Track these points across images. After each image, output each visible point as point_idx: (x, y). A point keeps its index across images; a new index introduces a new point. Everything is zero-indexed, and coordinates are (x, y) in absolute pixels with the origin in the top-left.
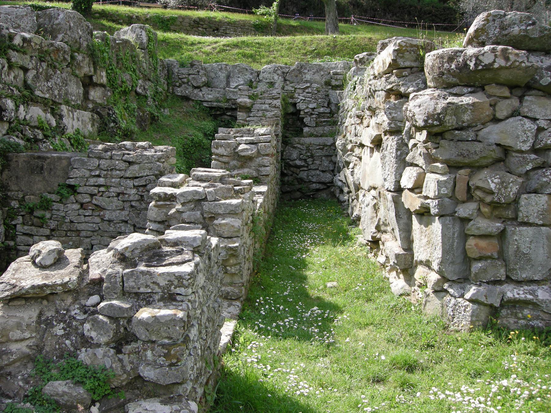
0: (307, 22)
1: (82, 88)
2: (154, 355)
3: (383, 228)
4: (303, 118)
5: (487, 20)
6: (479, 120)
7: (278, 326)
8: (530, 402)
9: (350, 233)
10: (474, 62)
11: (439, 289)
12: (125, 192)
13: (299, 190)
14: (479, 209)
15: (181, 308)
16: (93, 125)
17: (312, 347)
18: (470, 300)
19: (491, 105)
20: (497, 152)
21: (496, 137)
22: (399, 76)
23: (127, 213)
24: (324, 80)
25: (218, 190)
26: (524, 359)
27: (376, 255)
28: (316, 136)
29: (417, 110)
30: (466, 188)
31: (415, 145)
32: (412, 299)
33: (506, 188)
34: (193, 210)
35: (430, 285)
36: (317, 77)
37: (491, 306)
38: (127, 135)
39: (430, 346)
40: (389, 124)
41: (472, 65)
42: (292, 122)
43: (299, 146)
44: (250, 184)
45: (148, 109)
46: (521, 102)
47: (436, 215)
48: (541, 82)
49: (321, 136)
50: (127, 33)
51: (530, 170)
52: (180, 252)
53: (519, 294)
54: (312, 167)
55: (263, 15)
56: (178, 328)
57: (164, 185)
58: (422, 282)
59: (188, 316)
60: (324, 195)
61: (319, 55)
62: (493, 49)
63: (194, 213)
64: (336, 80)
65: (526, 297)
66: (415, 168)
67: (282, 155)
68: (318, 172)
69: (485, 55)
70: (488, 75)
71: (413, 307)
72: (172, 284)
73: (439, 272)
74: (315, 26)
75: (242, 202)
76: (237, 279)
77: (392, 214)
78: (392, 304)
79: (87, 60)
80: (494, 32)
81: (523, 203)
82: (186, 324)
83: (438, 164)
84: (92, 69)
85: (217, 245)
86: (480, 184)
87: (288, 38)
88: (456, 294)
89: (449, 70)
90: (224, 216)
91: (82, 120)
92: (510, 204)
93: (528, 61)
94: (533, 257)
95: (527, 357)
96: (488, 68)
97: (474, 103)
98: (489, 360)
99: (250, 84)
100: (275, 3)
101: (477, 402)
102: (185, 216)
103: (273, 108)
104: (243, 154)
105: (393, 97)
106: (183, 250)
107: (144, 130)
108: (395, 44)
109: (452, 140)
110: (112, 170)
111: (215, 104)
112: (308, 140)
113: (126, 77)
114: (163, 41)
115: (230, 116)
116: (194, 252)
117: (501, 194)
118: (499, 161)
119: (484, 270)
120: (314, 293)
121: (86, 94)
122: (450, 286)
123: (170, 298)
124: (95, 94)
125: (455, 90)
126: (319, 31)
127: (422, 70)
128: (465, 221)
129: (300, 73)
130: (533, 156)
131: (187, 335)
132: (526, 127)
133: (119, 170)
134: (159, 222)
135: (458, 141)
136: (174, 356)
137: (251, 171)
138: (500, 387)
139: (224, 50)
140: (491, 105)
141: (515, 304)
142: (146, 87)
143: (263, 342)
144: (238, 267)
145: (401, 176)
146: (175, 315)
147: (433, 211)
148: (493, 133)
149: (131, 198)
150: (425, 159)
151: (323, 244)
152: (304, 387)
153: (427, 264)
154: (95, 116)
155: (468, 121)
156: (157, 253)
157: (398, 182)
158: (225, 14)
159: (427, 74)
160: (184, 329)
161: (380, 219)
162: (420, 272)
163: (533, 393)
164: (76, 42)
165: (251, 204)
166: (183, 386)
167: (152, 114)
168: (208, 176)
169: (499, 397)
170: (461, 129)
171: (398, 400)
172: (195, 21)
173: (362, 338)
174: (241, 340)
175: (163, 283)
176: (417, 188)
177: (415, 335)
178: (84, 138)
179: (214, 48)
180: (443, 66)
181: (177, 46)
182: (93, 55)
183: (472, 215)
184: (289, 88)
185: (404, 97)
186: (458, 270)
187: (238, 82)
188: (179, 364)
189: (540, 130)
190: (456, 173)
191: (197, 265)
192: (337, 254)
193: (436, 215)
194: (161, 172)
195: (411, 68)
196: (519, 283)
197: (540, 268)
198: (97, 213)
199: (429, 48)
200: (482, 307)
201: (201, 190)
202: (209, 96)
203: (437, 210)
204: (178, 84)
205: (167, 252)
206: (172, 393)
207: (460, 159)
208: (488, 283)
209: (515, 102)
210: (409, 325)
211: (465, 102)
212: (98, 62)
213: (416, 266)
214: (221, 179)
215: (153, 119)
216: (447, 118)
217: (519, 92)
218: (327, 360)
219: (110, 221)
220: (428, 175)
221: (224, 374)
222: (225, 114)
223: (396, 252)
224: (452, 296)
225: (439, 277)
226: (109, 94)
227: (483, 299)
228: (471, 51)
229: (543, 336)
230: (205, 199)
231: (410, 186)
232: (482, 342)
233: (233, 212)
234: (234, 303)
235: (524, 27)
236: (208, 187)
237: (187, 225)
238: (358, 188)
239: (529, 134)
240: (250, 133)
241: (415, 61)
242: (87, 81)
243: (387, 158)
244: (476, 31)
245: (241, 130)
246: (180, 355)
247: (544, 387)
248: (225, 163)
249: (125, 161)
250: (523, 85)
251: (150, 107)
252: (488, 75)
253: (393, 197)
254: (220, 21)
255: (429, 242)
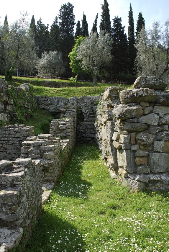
0: (88, 83)
1: (3, 105)
2: (6, 209)
3: (108, 154)
4: (84, 115)
5: (140, 79)
6: (138, 115)
7: (67, 192)
8: (159, 221)
9: (99, 156)
10: (136, 94)
11: (126, 176)
12: (15, 143)
13: (83, 140)
14: (140, 147)
15: (17, 190)
16: (7, 119)
17: (79, 200)
18: (137, 181)
19: (142, 109)
20: (145, 126)
21: (144, 120)
22: (111, 100)
23: (15, 150)
24: (91, 102)
25: (46, 142)
26: (157, 202)
27: (106, 164)
28: (89, 121)
29: (116, 112)
30: (135, 140)
31: (117, 124)
32: (118, 180)
33: (149, 139)
34: (37, 149)
35: (123, 175)
36: (88, 101)
37: (145, 182)
38: (21, 122)
39: (122, 198)
40: (108, 117)
41: (135, 95)
42: (80, 117)
43: (82, 125)
44: (59, 139)
45: (29, 113)
46: (153, 108)
47: (124, 150)
48: (160, 101)
49: (90, 121)
50: (22, 87)
51: (157, 132)
52: (20, 167)
53: (155, 178)
54: (87, 132)
55: (72, 80)
56: (15, 198)
57: (28, 140)
58: (121, 174)
59: (20, 193)
60: (92, 142)
61: (90, 94)
62: (143, 89)
63: (37, 150)
64: (95, 102)
65: (158, 179)
66: (117, 133)
67: (77, 128)
68: (89, 134)
69: (140, 91)
70: (141, 99)
71: (117, 183)
72: (14, 180)
73: (126, 170)
74: (90, 84)
75: (55, 146)
76: (53, 175)
77: (110, 149)
78: (110, 182)
79: (5, 95)
80: (143, 83)
81: (155, 144)
82: (20, 195)
83: (124, 131)
84: (7, 99)
85: (39, 164)
86: (139, 138)
87: (80, 88)
88: (132, 178)
89: (127, 97)
90: (48, 151)
91: (3, 117)
92: (151, 145)
93: (155, 93)
94: (160, 164)
95: (158, 202)
96: (141, 96)
97: (136, 109)
98: (144, 204)
99: (66, 104)
100: (76, 76)
101: (138, 222)
102: (34, 151)
103: (73, 112)
104: (61, 128)
105: (110, 107)
106: (21, 166)
107: (27, 120)
108: (110, 89)
109: (129, 122)
110: (10, 135)
111: (54, 111)
112: (86, 123)
113: (21, 101)
114: (37, 89)
115: (59, 115)
116: (25, 167)
117: (147, 142)
118: (146, 129)
119: (142, 169)
120: (83, 178)
121: (5, 108)
122: (130, 175)
123: (13, 186)
124: (9, 108)
125: (130, 104)
126: (91, 86)
127: (119, 98)
128: (134, 151)
129: (83, 100)
130: (158, 127)
131: (20, 201)
132: (155, 117)
133: (13, 135)
134: (25, 154)
135: (131, 122)
136: (13, 210)
137: (64, 134)
138: (147, 215)
139: (58, 92)
140: (142, 109)
141: (154, 182)
142: (29, 105)
143: (61, 198)
144: (53, 170)
145: (113, 136)
146: (14, 193)
147: (123, 148)
148: (143, 119)
149: (17, 145)
150: (120, 129)
151: (89, 160)
152: (72, 217)
153: (122, 167)
154: (9, 115)
155: (135, 115)
156: (10, 168)
157: (111, 138)
158: (59, 80)
159: (120, 99)
160: (17, 198)
161: (107, 151)
162: (120, 170)
163: (160, 217)
164: (1, 89)
165: (60, 147)
166: (18, 221)
167: (31, 114)
168: (43, 137)
169: (147, 219)
170: (132, 118)
171: (108, 221)
172: (48, 82)
173: (98, 196)
174: (52, 198)
175: (10, 180)
176: (118, 140)
177: (117, 194)
178: (4, 123)
179: (54, 92)
180: (125, 96)
181: (41, 91)
182: (8, 94)
183: (137, 149)
184: (79, 105)
185: (112, 107)
186: (133, 169)
187: (61, 103)
188: (15, 213)
189: (160, 118)
190: (131, 134)
191: (25, 173)
192: (93, 163)
193: (124, 150)
194: (28, 135)
195: (116, 97)
196: (155, 174)
197: (163, 168)
198: (5, 151)
199: (121, 90)
200: (142, 183)
201: (40, 142)
202: (51, 108)
203: (124, 148)
204: (40, 104)
205: (14, 167)
206: (13, 224)
207: (132, 129)
208: (144, 174)
209: (151, 108)
210: (115, 190)
211: (133, 109)
212: (10, 96)
213: (119, 168)
214: (49, 138)
215: (31, 116)
216: (127, 114)
217: (152, 105)
218: (84, 205)
219: (9, 153)
220: (121, 135)
221: (44, 212)
222: (57, 114)
223: (112, 163)
224: (131, 179)
225: (126, 172)
226: (14, 107)
227: (142, 180)
228: (135, 90)
229: (165, 194)
230: (41, 145)
231: (115, 139)
232: (142, 196)
233: (51, 150)
234: (52, 183)
235: (153, 81)
236: (43, 141)
237: (35, 155)
238: (101, 139)
239: (156, 119)
240: (63, 121)
241: (117, 94)
242: (6, 103)
243: (108, 129)
244: (137, 83)
245: (60, 120)
246: (15, 209)
247: (164, 214)
248: (54, 131)
249: (15, 132)
250: (154, 102)
251: (30, 112)
252: (141, 99)
253: (110, 143)
254: (57, 83)
255: (122, 159)
